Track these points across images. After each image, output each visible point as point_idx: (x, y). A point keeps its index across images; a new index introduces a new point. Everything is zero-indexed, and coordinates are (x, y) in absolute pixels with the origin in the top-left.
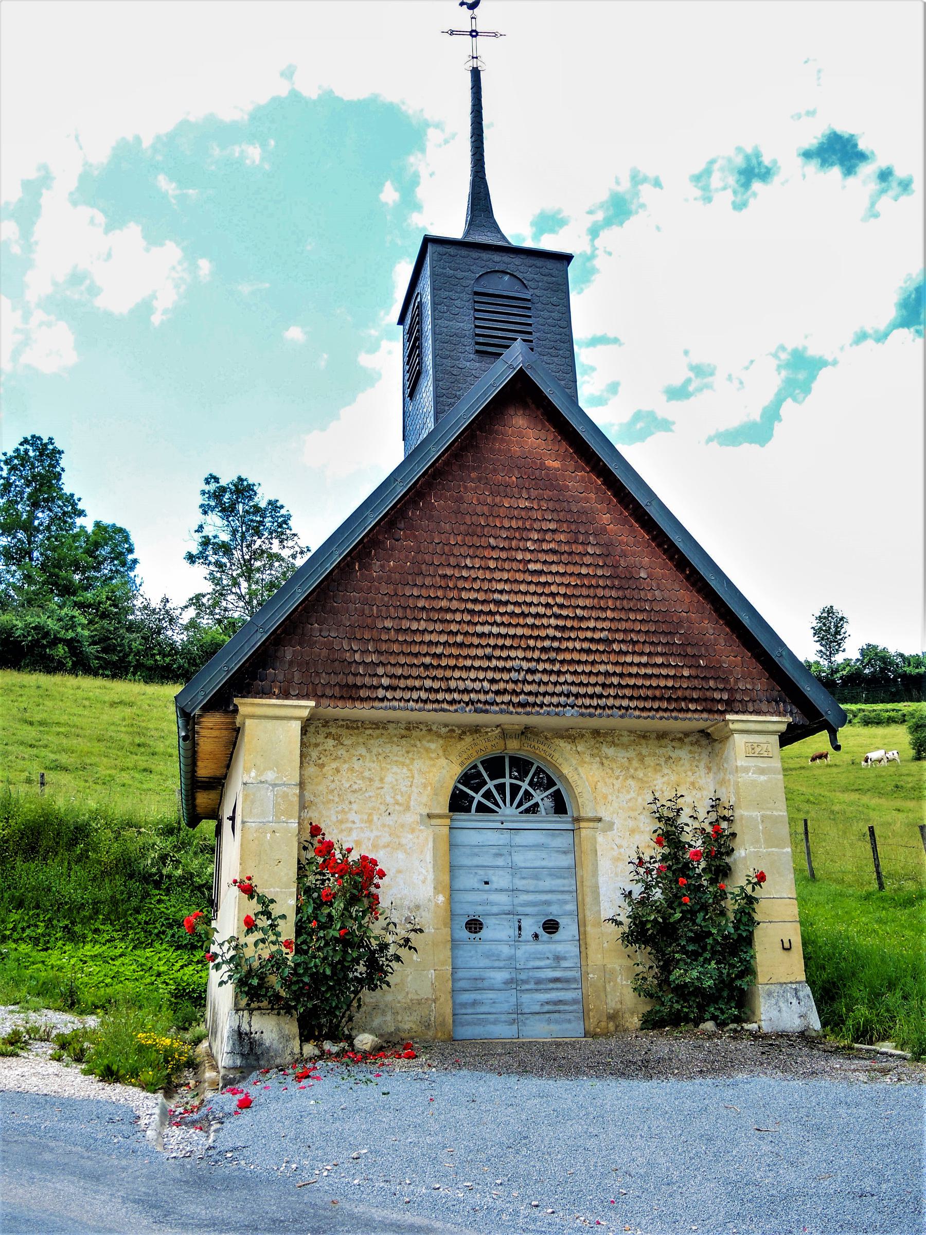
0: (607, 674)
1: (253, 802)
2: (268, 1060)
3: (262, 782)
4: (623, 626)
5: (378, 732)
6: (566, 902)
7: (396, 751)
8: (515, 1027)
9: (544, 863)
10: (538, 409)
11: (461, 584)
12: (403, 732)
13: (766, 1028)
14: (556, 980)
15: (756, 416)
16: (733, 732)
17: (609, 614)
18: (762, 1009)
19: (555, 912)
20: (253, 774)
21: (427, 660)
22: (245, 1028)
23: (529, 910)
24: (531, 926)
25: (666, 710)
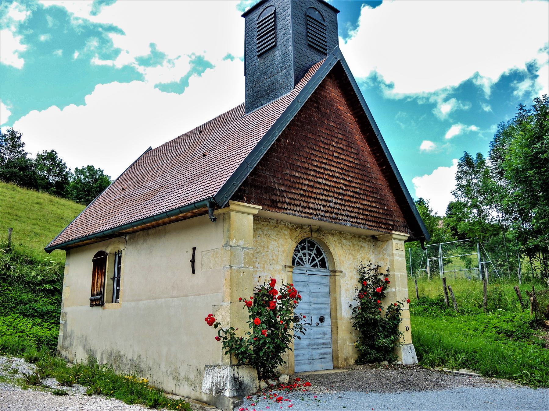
0: (359, 208)
1: (235, 256)
2: (247, 392)
3: (238, 246)
4: (363, 187)
5: (266, 223)
6: (326, 308)
7: (273, 233)
8: (311, 365)
9: (319, 290)
10: (336, 80)
11: (313, 158)
12: (275, 224)
13: (404, 364)
14: (324, 344)
15: (178, 80)
16: (392, 238)
17: (359, 181)
18: (403, 355)
19: (323, 313)
20: (234, 241)
21: (302, 192)
22: (236, 375)
23: (315, 312)
24: (316, 320)
25: (376, 227)
